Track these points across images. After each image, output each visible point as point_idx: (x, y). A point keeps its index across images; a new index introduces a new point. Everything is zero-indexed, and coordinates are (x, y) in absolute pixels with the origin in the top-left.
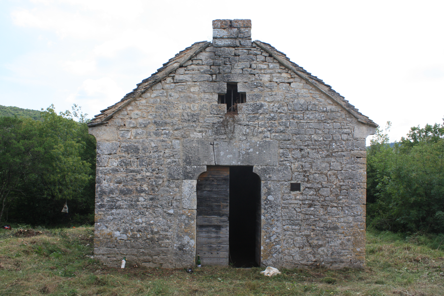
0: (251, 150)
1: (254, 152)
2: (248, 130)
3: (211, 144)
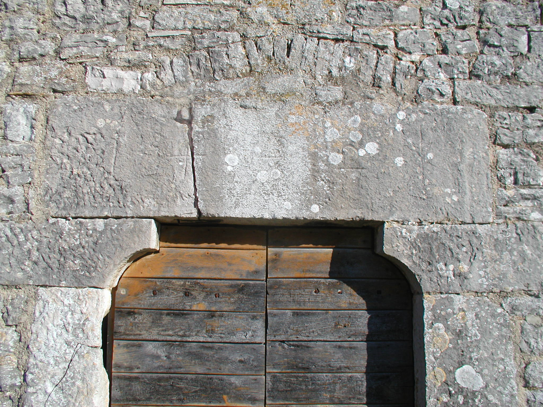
0: (372, 148)
1: (383, 157)
2: (350, 63)
3: (179, 119)
